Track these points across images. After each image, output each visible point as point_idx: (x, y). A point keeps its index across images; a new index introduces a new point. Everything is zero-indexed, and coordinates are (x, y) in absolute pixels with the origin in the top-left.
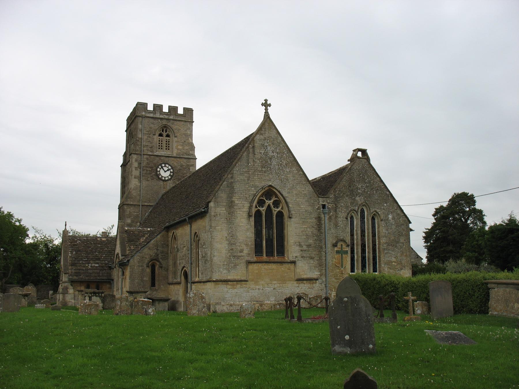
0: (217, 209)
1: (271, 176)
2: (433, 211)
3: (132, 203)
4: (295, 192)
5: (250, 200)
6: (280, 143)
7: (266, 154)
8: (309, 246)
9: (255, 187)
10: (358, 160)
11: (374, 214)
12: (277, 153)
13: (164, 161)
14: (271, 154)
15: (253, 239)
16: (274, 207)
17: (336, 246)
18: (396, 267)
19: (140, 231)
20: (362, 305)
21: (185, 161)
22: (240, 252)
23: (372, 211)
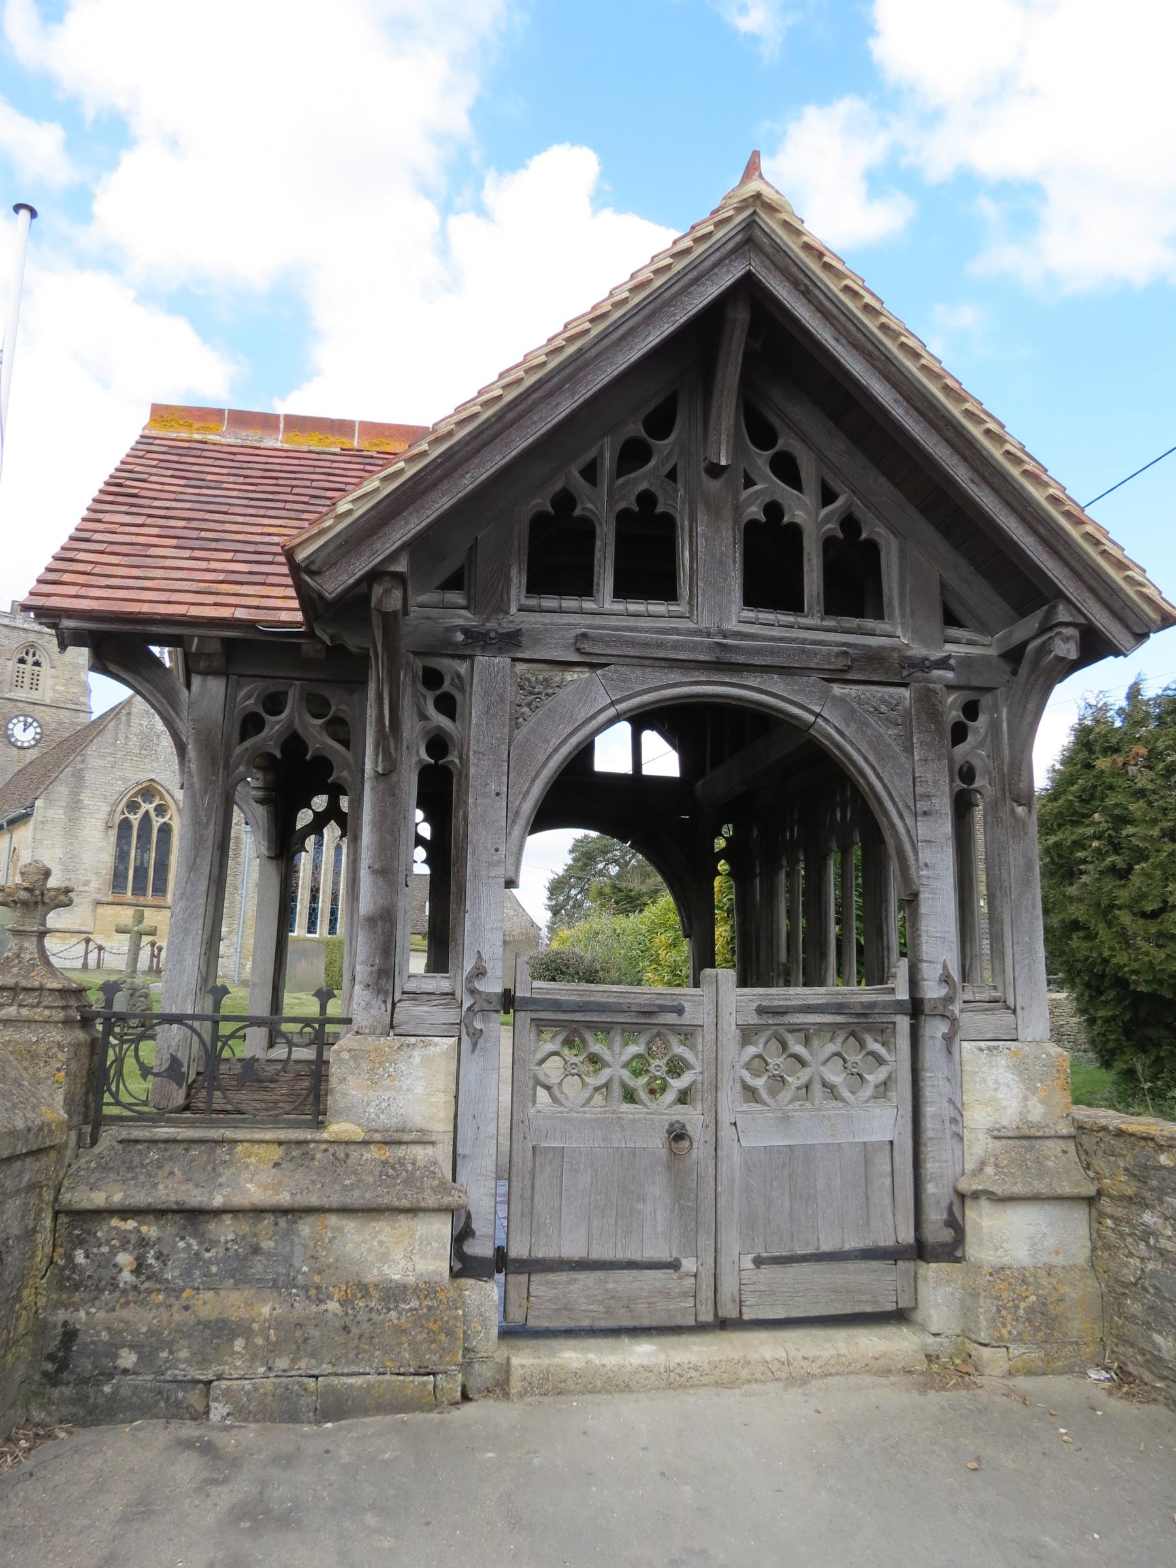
1: (155, 764)
2: (569, 846)
21: (68, 714)
22: (85, 885)
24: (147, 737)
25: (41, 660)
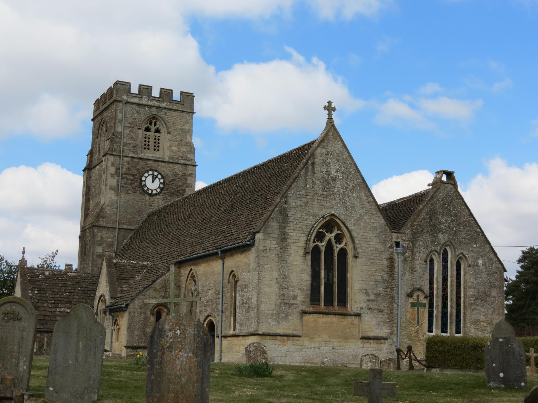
0: (267, 242)
1: (333, 202)
3: (105, 225)
4: (362, 224)
5: (307, 233)
6: (346, 160)
7: (329, 173)
8: (378, 295)
9: (315, 215)
10: (443, 185)
11: (460, 258)
12: (342, 172)
13: (152, 166)
14: (334, 173)
15: (309, 282)
16: (336, 243)
17: (412, 297)
18: (486, 328)
19: (134, 266)
21: (180, 167)
22: (294, 299)
23: (457, 253)
24: (326, 181)
25: (161, 128)
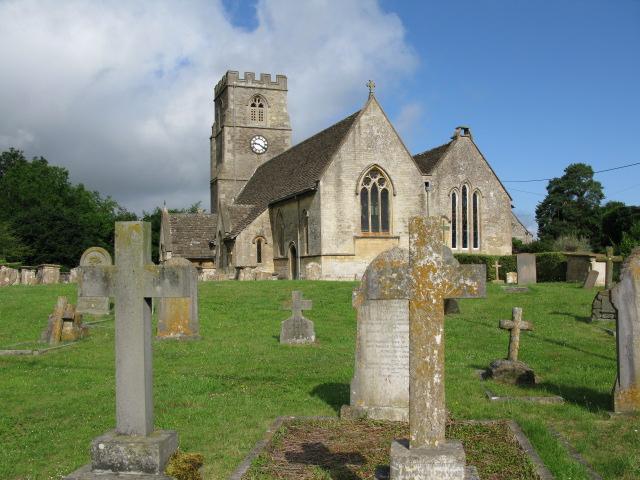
7: (371, 133)
9: (361, 166)
13: (259, 132)
20: (516, 354)
